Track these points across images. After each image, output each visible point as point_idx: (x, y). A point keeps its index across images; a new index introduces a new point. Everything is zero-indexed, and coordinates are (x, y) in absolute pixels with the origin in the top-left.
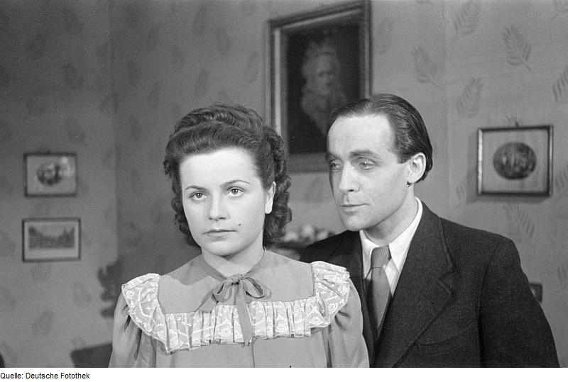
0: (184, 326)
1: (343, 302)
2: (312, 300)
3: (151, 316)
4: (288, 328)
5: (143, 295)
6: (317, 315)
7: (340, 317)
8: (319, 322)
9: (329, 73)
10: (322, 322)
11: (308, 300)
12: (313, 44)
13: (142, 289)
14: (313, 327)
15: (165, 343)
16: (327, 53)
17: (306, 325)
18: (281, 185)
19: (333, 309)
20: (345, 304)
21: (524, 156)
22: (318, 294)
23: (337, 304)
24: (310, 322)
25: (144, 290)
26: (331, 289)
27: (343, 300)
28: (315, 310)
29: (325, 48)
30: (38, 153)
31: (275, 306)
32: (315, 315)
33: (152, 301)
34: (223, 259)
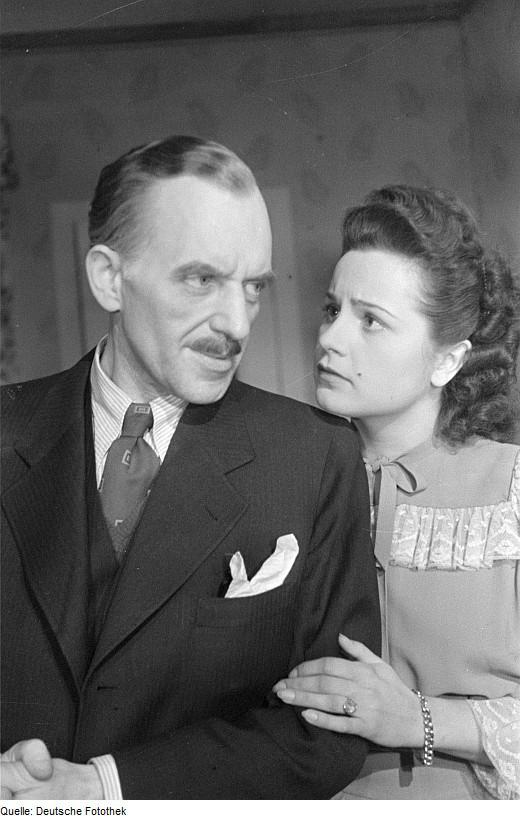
4: (449, 556)
31: (450, 564)
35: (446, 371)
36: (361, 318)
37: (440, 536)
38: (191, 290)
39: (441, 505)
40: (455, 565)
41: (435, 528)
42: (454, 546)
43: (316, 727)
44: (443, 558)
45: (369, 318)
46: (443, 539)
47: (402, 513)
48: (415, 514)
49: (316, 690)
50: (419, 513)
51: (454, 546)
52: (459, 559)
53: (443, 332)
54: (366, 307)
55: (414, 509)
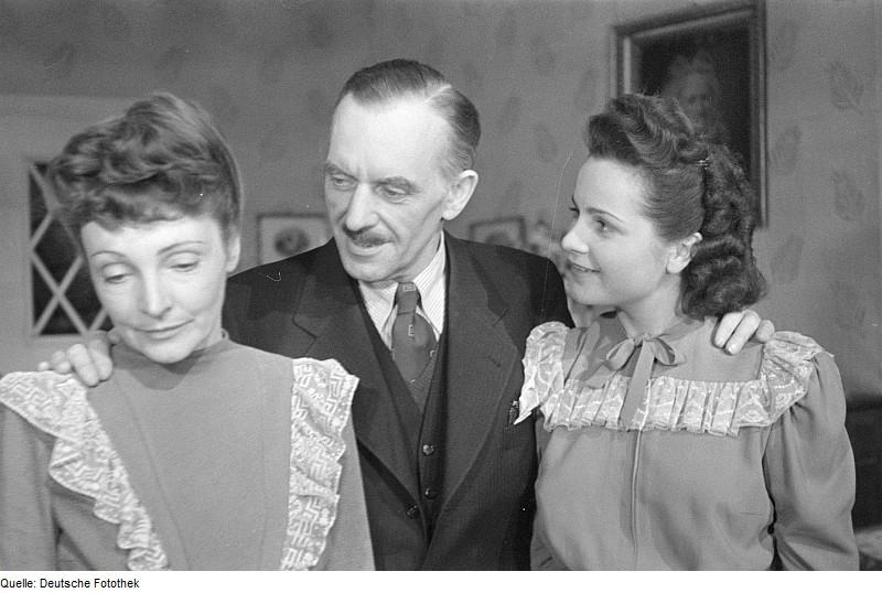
0: (570, 397)
1: (800, 391)
2: (754, 385)
3: (549, 384)
4: (699, 420)
5: (545, 353)
6: (756, 408)
7: (797, 411)
8: (758, 418)
9: (704, 97)
10: (762, 419)
11: (747, 384)
12: (680, 58)
13: (543, 345)
14: (743, 425)
15: (547, 418)
16: (700, 71)
17: (736, 420)
18: (731, 237)
19: (784, 401)
20: (804, 394)
21: (740, 162)
22: (763, 377)
23: (790, 395)
24: (743, 417)
25: (546, 347)
26: (783, 369)
27: (802, 388)
28: (756, 399)
29: (697, 63)
30: (275, 215)
31: (694, 387)
32: (753, 407)
33: (553, 364)
34: (164, 371)
35: (678, 260)
36: (448, 120)
37: (692, 402)
38: (669, 181)
39: (694, 377)
40: (704, 428)
41: (690, 397)
42: (705, 413)
43: (329, 144)
44: (693, 420)
45: (603, 223)
46: (696, 404)
47: (661, 383)
48: (672, 384)
49: (228, 191)
50: (676, 385)
51: (705, 413)
52: (707, 424)
53: (671, 229)
54: (599, 214)
55: (672, 381)
